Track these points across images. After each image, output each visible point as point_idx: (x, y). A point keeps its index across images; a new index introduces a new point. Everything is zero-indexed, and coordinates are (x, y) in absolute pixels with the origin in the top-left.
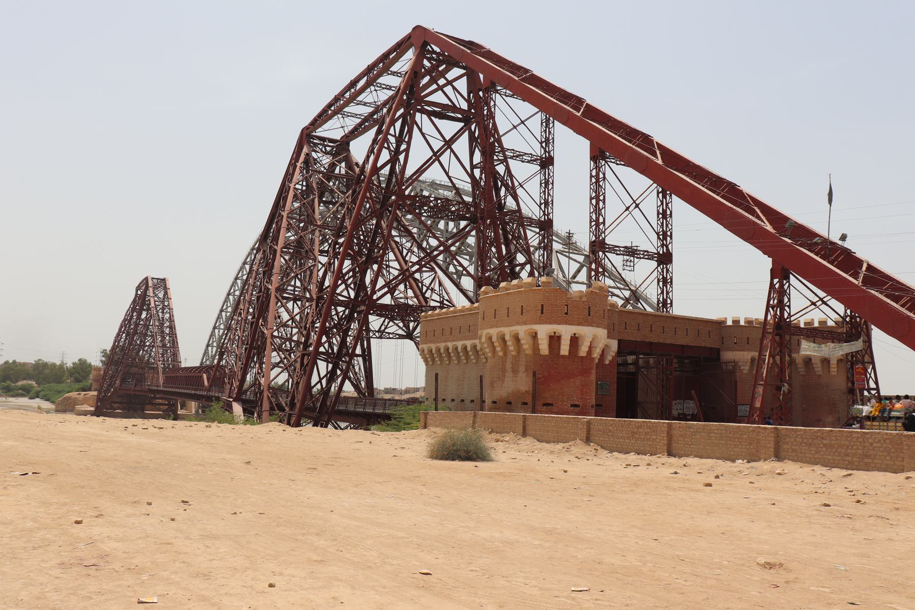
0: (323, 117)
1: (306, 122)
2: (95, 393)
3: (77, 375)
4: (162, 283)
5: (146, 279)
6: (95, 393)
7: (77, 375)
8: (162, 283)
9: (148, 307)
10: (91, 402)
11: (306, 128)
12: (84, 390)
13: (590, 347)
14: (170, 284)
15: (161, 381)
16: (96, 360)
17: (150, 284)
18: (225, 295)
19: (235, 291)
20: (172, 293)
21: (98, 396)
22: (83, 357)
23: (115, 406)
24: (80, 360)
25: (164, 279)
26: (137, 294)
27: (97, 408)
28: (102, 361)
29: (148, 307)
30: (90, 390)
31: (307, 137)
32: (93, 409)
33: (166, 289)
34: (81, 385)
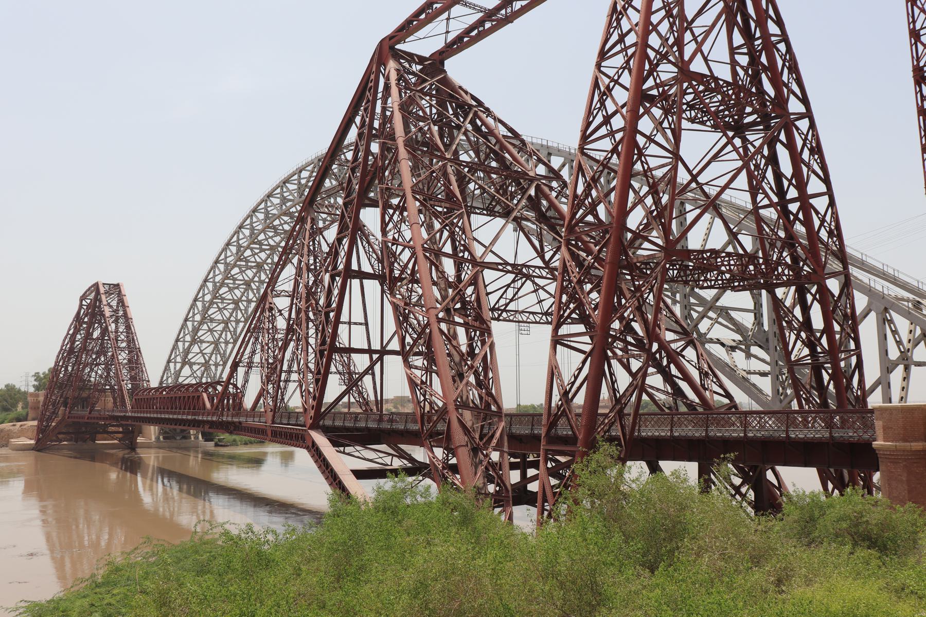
0: (407, 28)
1: (389, 29)
2: (35, 423)
3: (5, 403)
4: (115, 289)
5: (96, 285)
6: (35, 423)
7: (5, 403)
8: (115, 289)
9: (100, 315)
10: (30, 434)
11: (391, 37)
12: (19, 420)
13: (476, 474)
14: (125, 290)
15: (129, 407)
16: (26, 384)
17: (102, 290)
18: (181, 321)
19: (194, 315)
20: (129, 300)
21: (38, 426)
22: (11, 382)
23: (61, 436)
24: (7, 386)
25: (118, 285)
26: (81, 306)
27: (38, 441)
28: (34, 386)
29: (100, 315)
30: (26, 420)
31: (387, 49)
32: (33, 442)
33: (120, 295)
34: (12, 415)
